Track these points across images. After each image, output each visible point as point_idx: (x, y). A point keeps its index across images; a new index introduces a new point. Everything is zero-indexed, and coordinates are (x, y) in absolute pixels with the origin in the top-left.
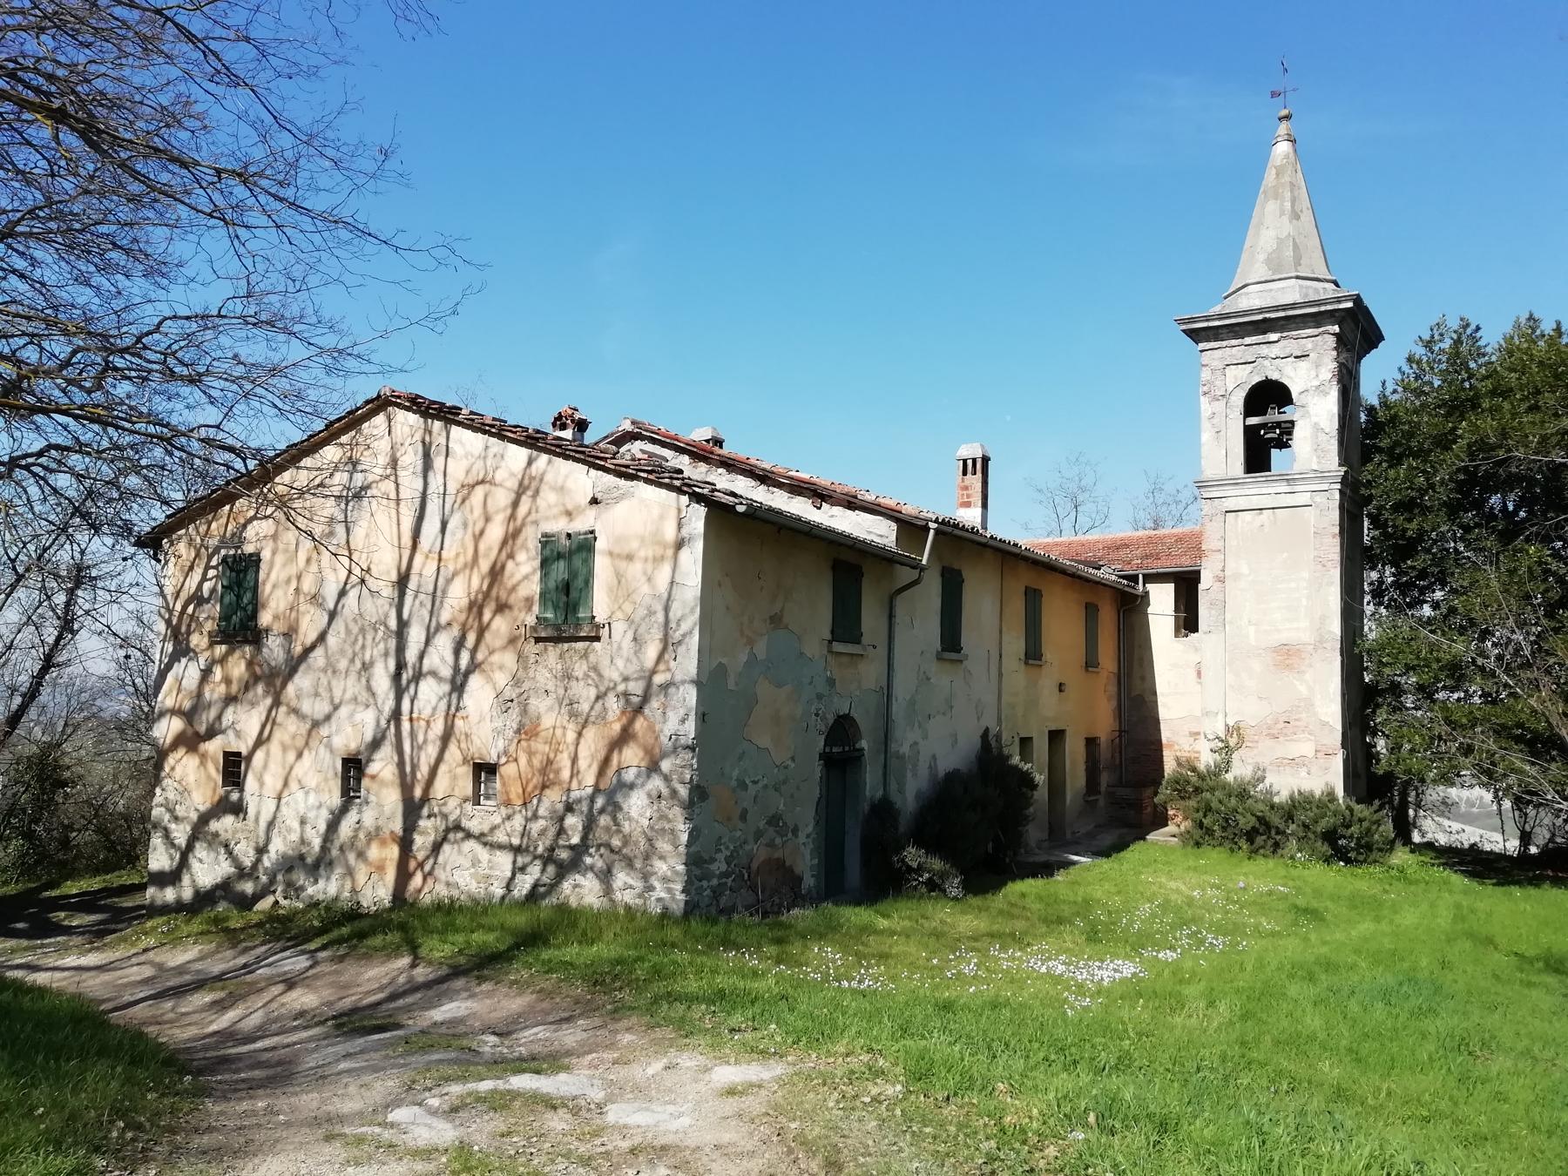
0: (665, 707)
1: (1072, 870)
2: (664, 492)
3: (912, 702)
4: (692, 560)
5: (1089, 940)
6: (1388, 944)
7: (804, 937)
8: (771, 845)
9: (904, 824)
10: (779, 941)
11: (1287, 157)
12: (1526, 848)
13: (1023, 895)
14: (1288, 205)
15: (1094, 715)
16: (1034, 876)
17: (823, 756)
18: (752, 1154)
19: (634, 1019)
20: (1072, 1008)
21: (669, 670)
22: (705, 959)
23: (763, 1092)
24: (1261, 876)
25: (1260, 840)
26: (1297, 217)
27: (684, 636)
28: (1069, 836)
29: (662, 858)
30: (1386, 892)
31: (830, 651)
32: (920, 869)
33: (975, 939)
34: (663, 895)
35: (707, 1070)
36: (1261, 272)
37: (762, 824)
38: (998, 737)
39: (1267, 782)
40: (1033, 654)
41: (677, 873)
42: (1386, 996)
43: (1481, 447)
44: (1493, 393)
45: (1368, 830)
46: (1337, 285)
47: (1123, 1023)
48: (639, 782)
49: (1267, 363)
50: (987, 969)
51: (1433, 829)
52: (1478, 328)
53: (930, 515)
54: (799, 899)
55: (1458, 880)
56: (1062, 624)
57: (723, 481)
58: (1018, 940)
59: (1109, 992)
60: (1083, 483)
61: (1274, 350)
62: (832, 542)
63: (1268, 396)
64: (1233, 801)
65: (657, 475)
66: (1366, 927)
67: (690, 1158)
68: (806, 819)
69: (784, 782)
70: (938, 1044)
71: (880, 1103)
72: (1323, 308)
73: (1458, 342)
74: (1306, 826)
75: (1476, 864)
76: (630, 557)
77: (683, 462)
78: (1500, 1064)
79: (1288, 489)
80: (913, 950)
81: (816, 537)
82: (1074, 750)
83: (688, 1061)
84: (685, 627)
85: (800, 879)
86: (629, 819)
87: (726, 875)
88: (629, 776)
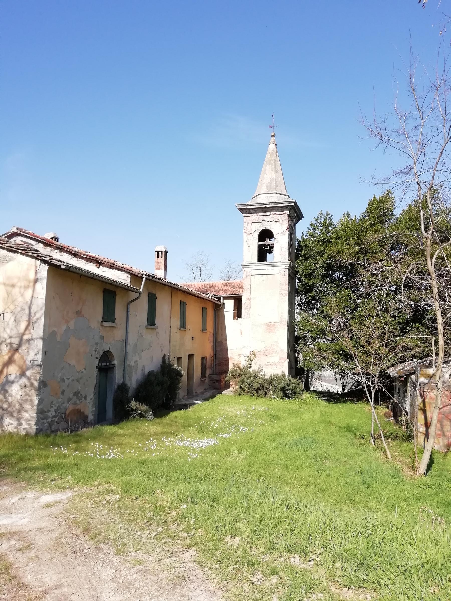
0: (28, 348)
1: (195, 406)
2: (29, 259)
3: (135, 345)
4: (41, 289)
5: (199, 432)
6: (299, 426)
7: (87, 440)
8: (75, 403)
9: (130, 393)
10: (76, 442)
11: (273, 150)
12: (344, 391)
13: (176, 417)
14: (273, 167)
15: (204, 348)
16: (181, 409)
17: (97, 367)
18: (53, 530)
19: (8, 480)
20: (191, 458)
21: (30, 333)
22: (43, 452)
23: (62, 504)
24: (259, 405)
25: (260, 392)
26: (277, 172)
27: (37, 319)
28: (194, 394)
29: (26, 411)
30: (300, 408)
31: (102, 326)
32: (136, 410)
33: (156, 435)
34: (26, 427)
35: (38, 498)
36: (264, 190)
37: (71, 396)
38: (169, 358)
39: (263, 371)
40: (183, 326)
41: (32, 417)
42: (296, 444)
43: (330, 257)
44: (336, 238)
45: (295, 387)
46: (289, 197)
47: (208, 462)
48: (16, 380)
49: (266, 223)
50: (160, 446)
51: (318, 385)
52: (332, 216)
53: (143, 273)
54: (86, 424)
55: (322, 402)
56: (194, 314)
57: (56, 255)
58: (173, 434)
59: (205, 450)
60: (203, 263)
61: (268, 218)
62: (103, 282)
63: (266, 234)
64: (252, 378)
65: (26, 251)
66: (293, 420)
67: (26, 535)
68: (90, 394)
69: (81, 378)
70: (135, 478)
71: (109, 503)
72: (284, 205)
73: (326, 220)
74: (275, 386)
75: (329, 397)
76: (13, 286)
77: (40, 247)
78: (330, 463)
79: (272, 268)
80: (132, 441)
81: (96, 280)
82: (197, 362)
83: (30, 495)
84: (38, 315)
85: (87, 417)
86: (11, 396)
87: (55, 417)
88: (11, 378)
